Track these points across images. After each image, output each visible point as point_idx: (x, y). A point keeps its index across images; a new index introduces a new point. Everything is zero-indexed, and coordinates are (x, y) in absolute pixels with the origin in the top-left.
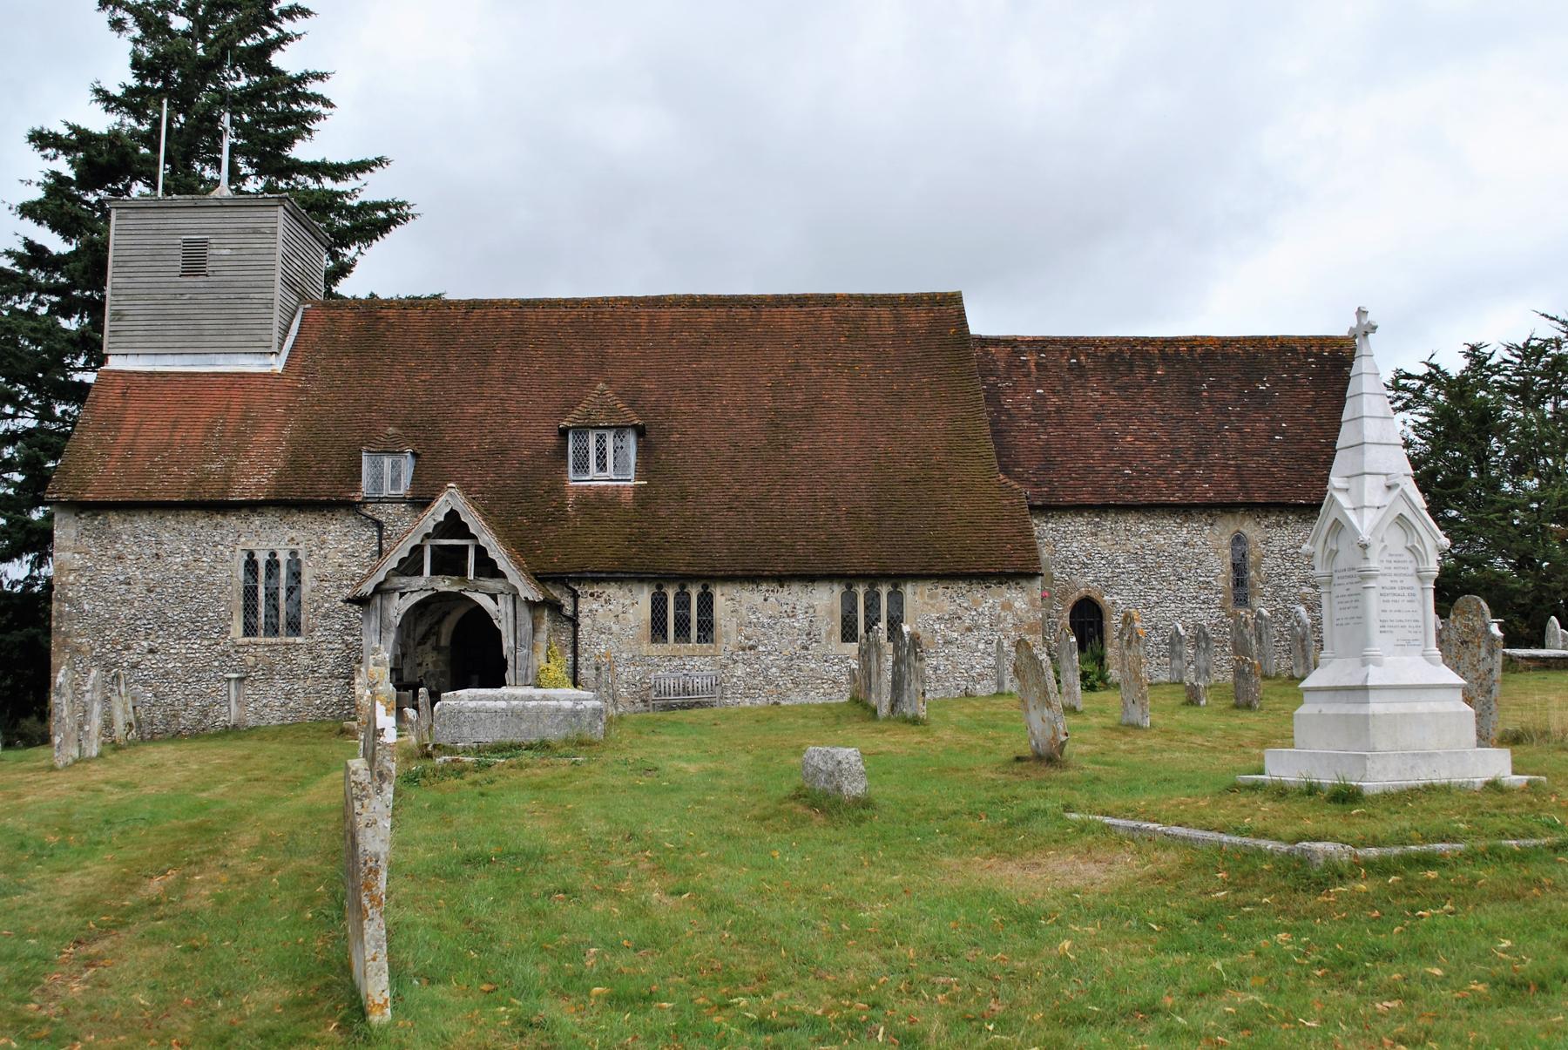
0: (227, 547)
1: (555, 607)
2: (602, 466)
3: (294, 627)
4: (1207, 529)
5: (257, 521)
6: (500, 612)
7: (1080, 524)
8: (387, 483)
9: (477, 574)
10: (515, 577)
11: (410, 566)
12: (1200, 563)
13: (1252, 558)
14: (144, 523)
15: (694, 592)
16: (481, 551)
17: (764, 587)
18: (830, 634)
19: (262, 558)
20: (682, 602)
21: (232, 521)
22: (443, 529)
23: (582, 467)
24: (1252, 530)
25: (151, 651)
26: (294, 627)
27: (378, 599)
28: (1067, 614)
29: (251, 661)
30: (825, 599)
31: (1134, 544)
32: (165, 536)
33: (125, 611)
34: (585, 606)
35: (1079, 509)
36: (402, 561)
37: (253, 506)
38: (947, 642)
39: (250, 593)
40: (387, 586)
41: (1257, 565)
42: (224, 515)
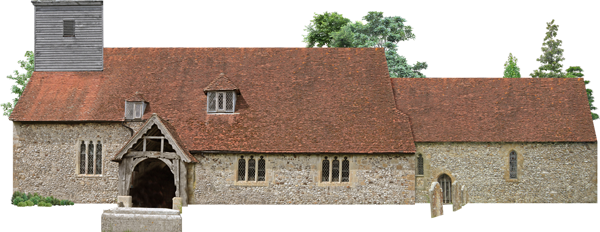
2: (221, 106)
3: (99, 171)
5: (85, 129)
6: (174, 167)
8: (135, 113)
9: (165, 151)
10: (179, 151)
11: (137, 147)
12: (494, 162)
13: (518, 160)
14: (44, 129)
16: (166, 141)
17: (288, 157)
18: (316, 178)
19: (87, 143)
21: (76, 128)
22: (149, 133)
23: (213, 107)
26: (99, 171)
27: (125, 161)
29: (82, 183)
30: (318, 162)
32: (52, 135)
33: (37, 163)
36: (134, 145)
37: (84, 123)
38: (371, 183)
39: (82, 157)
41: (523, 161)
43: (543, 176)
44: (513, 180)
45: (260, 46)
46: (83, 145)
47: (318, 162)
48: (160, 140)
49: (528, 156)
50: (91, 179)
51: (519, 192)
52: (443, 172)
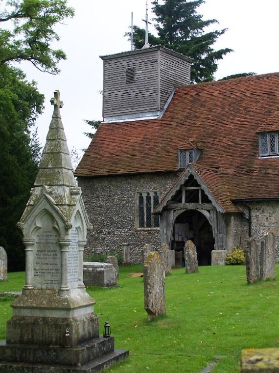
0: (132, 192)
1: (240, 216)
11: (177, 198)
14: (105, 183)
16: (203, 191)
19: (144, 195)
22: (187, 183)
25: (109, 233)
34: (254, 214)
39: (141, 209)
40: (168, 207)
42: (131, 179)
45: (188, 154)
46: (141, 198)
48: (198, 190)
50: (149, 232)
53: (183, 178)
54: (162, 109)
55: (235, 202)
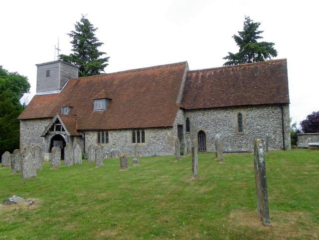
1: (80, 137)
4: (231, 112)
7: (200, 113)
11: (52, 129)
13: (243, 119)
14: (31, 122)
15: (141, 131)
20: (103, 135)
24: (244, 112)
28: (197, 135)
30: (129, 134)
31: (213, 117)
32: (34, 125)
34: (86, 136)
35: (199, 109)
41: (246, 120)
43: (258, 130)
44: (240, 133)
47: (129, 134)
49: (250, 116)
51: (244, 141)
52: (200, 129)
53: (54, 120)
54: (60, 89)
55: (78, 131)
